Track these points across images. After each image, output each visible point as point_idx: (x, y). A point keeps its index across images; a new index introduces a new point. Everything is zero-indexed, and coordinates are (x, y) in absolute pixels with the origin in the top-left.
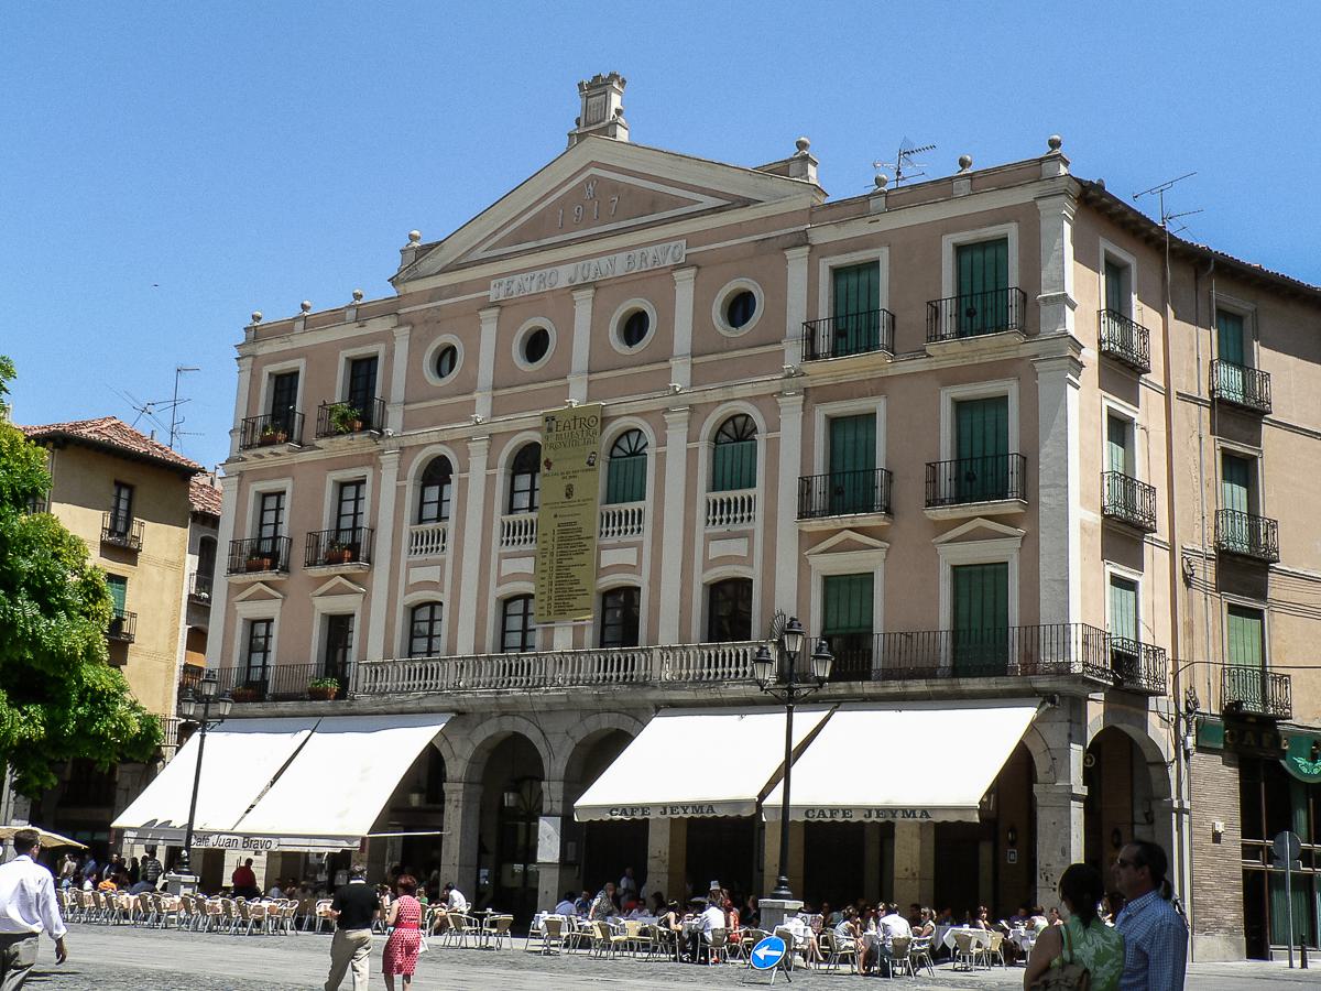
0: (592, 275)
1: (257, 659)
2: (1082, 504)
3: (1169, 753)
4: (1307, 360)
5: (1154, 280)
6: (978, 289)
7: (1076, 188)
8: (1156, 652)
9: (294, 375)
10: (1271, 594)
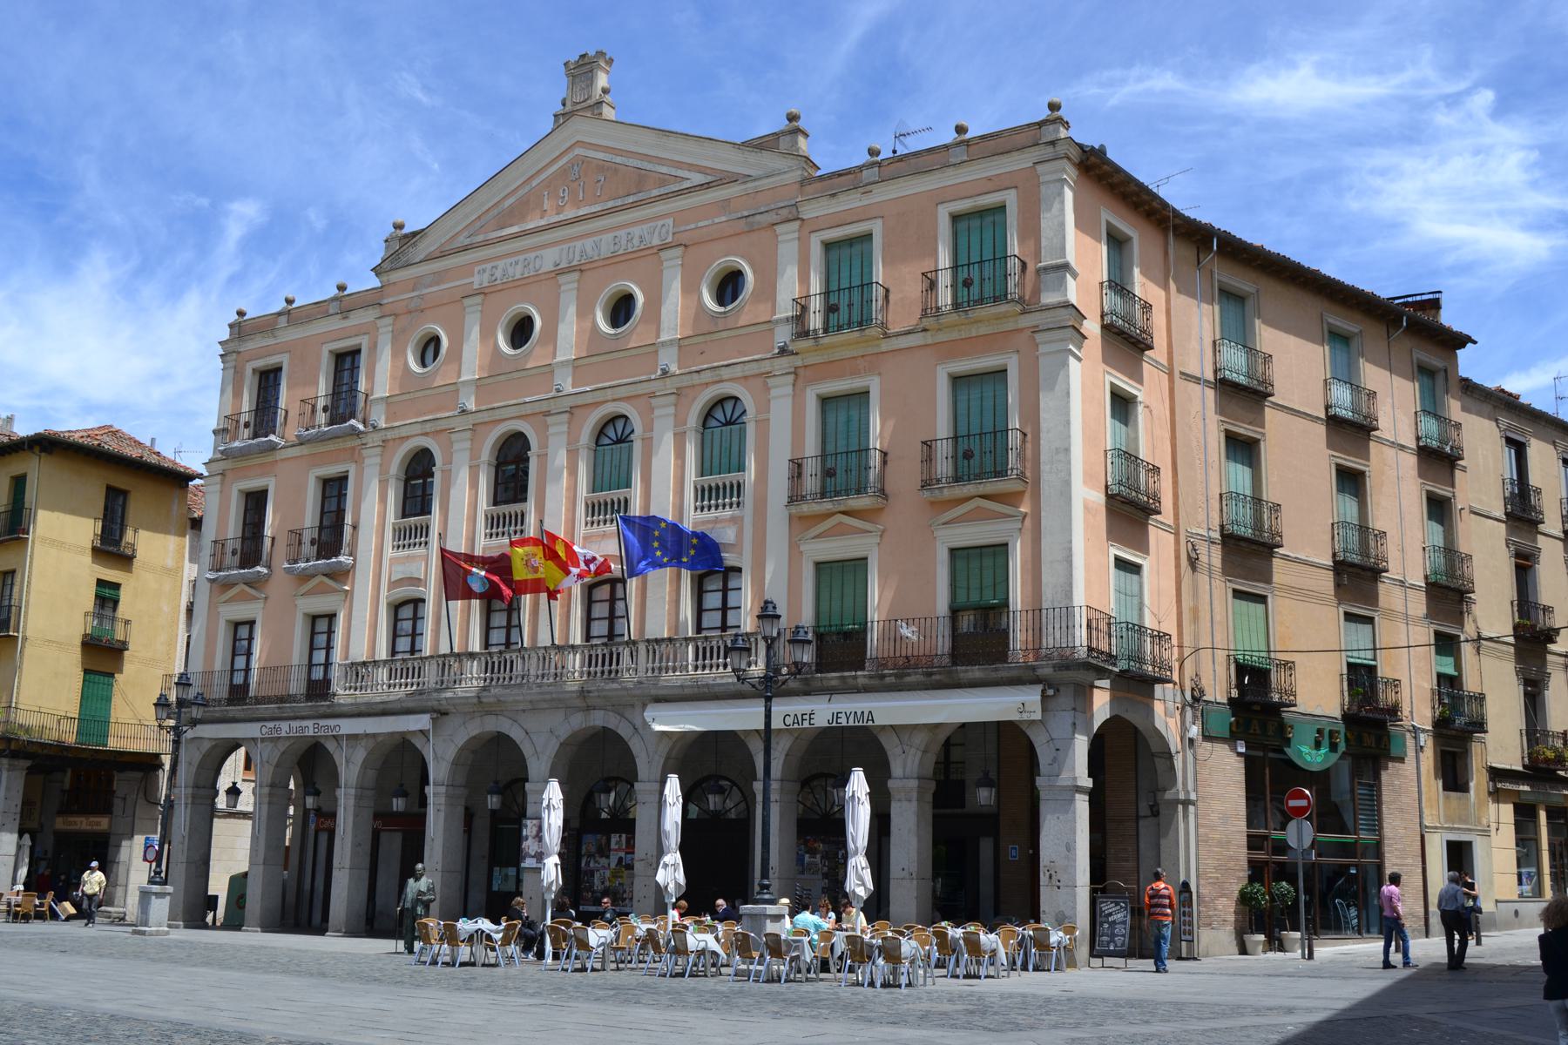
0: (577, 257)
1: (240, 662)
2: (1085, 482)
3: (1174, 742)
5: (1156, 252)
6: (975, 258)
7: (1075, 154)
8: (1161, 637)
9: (277, 370)
10: (1276, 578)
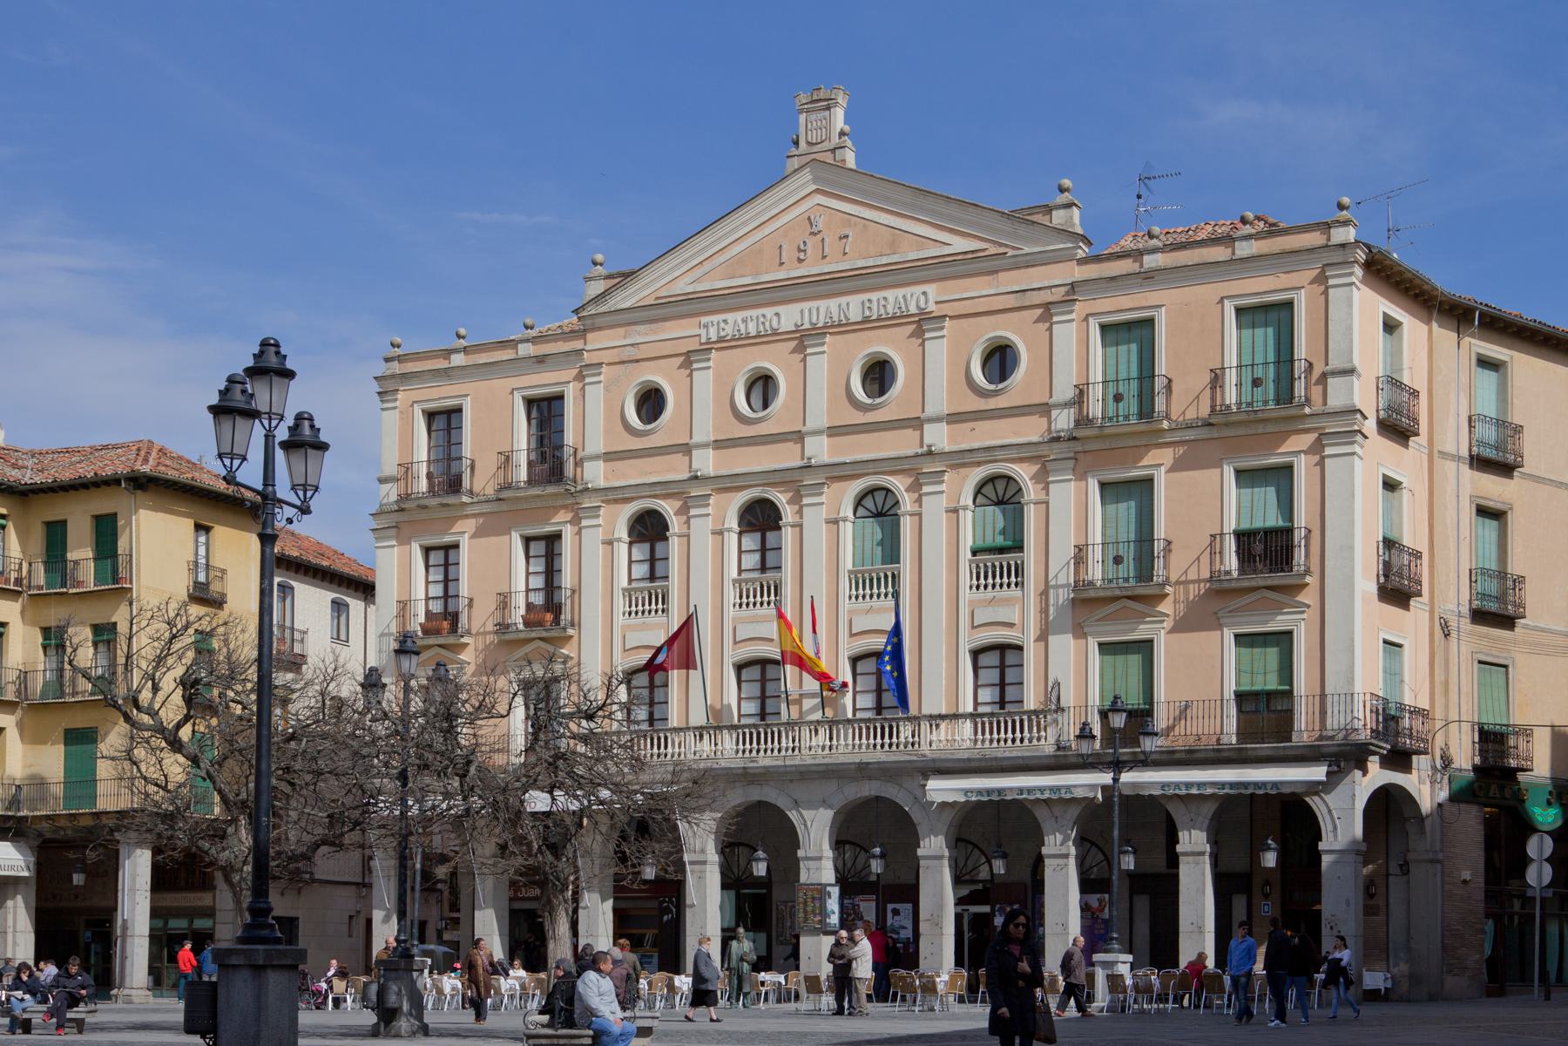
4: (489, 536)
